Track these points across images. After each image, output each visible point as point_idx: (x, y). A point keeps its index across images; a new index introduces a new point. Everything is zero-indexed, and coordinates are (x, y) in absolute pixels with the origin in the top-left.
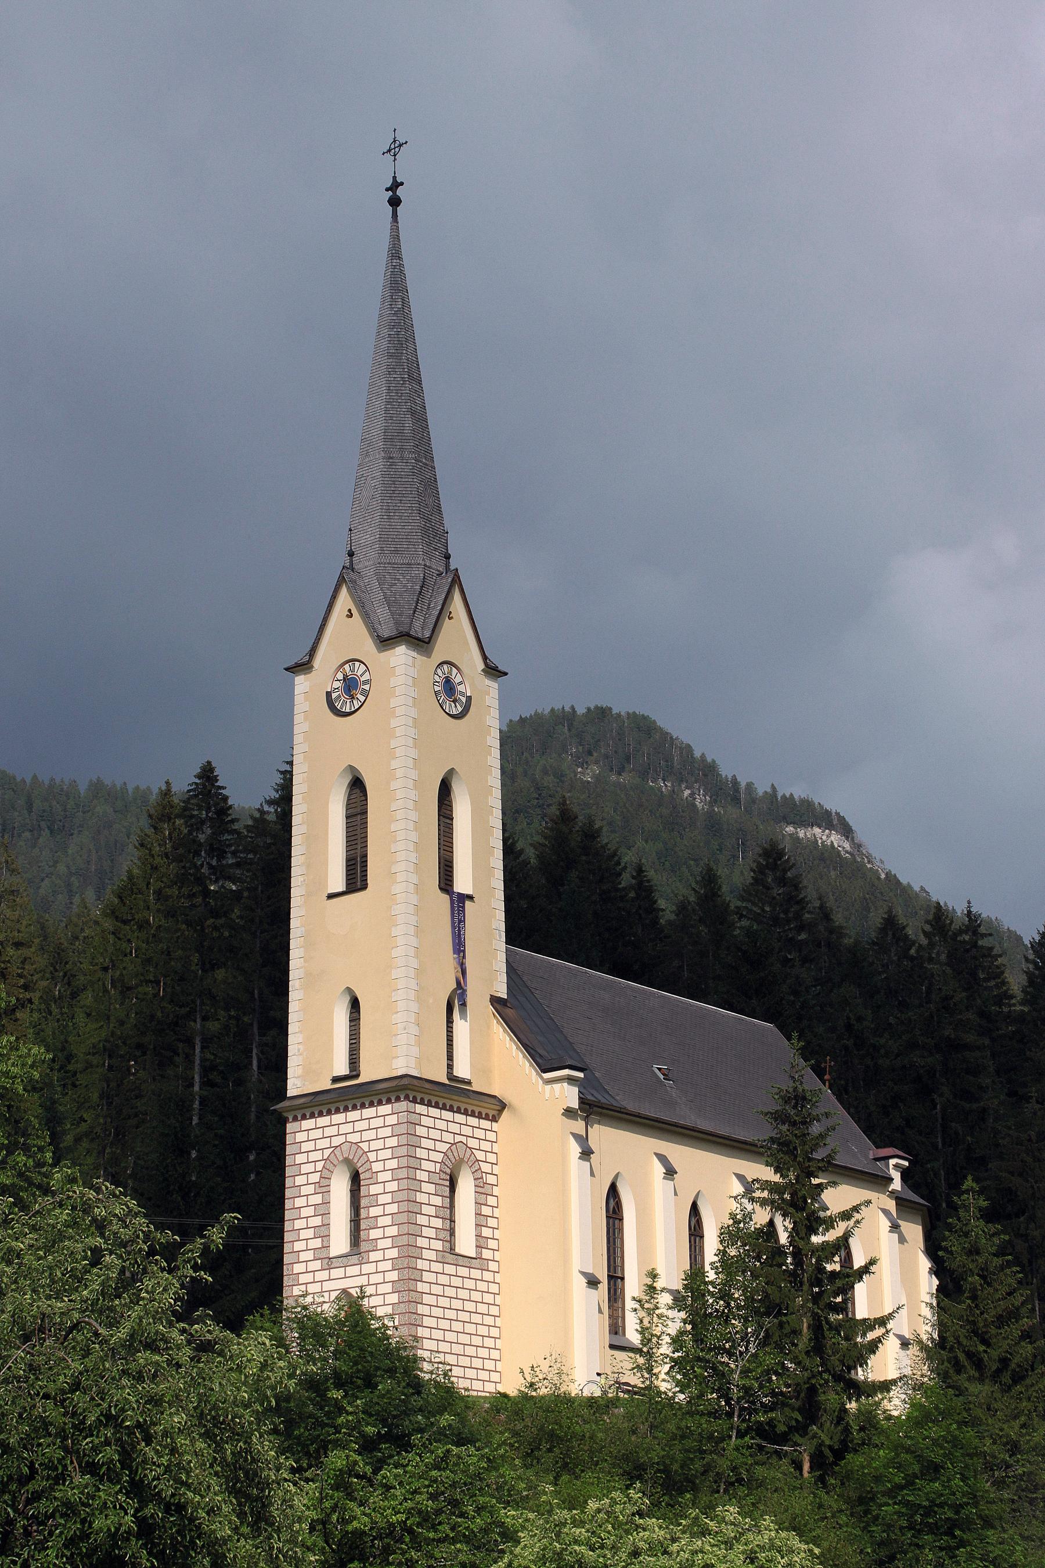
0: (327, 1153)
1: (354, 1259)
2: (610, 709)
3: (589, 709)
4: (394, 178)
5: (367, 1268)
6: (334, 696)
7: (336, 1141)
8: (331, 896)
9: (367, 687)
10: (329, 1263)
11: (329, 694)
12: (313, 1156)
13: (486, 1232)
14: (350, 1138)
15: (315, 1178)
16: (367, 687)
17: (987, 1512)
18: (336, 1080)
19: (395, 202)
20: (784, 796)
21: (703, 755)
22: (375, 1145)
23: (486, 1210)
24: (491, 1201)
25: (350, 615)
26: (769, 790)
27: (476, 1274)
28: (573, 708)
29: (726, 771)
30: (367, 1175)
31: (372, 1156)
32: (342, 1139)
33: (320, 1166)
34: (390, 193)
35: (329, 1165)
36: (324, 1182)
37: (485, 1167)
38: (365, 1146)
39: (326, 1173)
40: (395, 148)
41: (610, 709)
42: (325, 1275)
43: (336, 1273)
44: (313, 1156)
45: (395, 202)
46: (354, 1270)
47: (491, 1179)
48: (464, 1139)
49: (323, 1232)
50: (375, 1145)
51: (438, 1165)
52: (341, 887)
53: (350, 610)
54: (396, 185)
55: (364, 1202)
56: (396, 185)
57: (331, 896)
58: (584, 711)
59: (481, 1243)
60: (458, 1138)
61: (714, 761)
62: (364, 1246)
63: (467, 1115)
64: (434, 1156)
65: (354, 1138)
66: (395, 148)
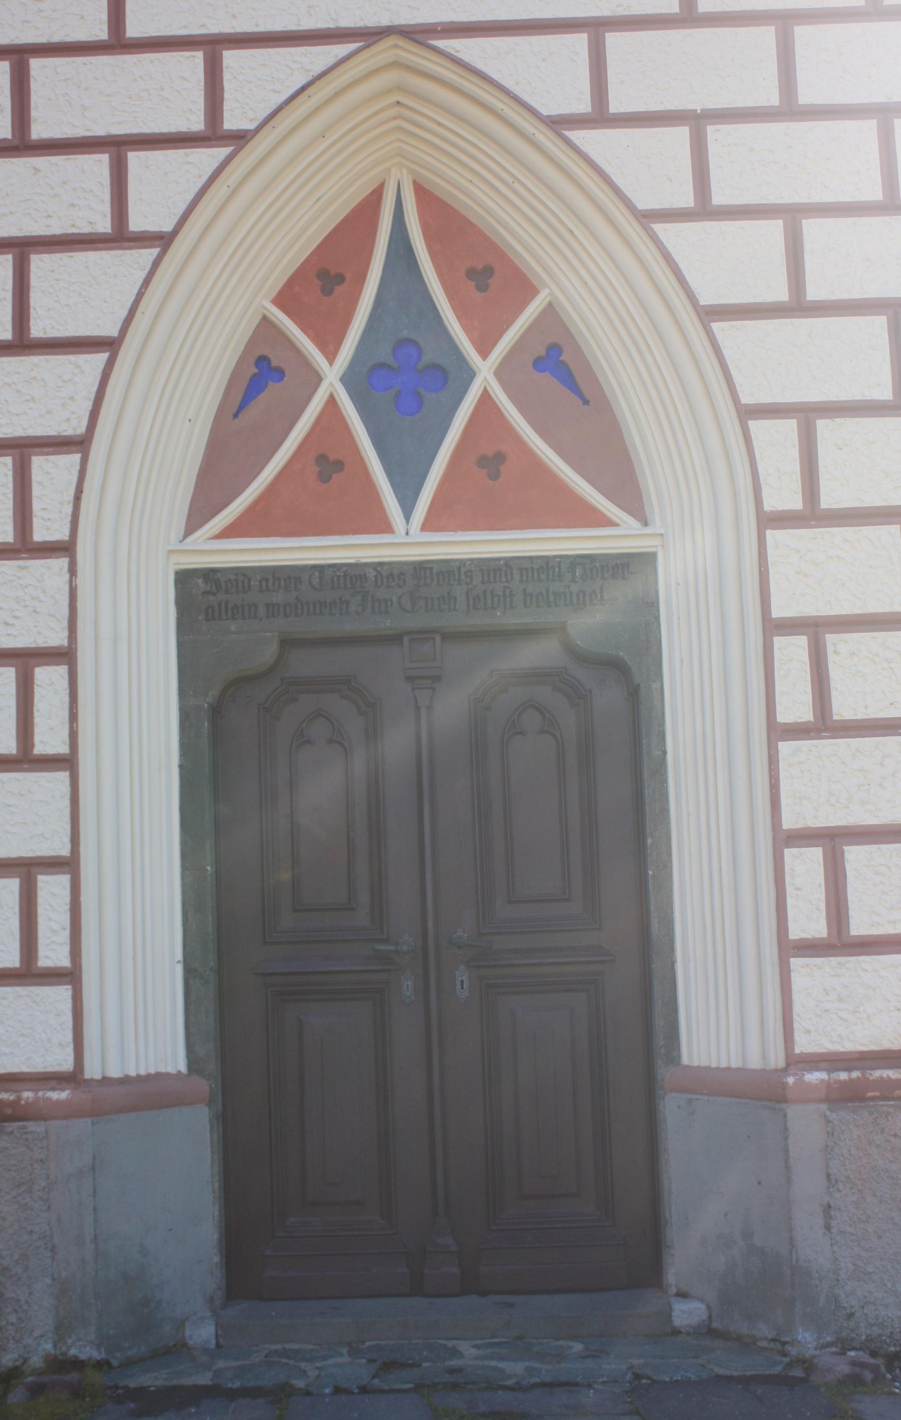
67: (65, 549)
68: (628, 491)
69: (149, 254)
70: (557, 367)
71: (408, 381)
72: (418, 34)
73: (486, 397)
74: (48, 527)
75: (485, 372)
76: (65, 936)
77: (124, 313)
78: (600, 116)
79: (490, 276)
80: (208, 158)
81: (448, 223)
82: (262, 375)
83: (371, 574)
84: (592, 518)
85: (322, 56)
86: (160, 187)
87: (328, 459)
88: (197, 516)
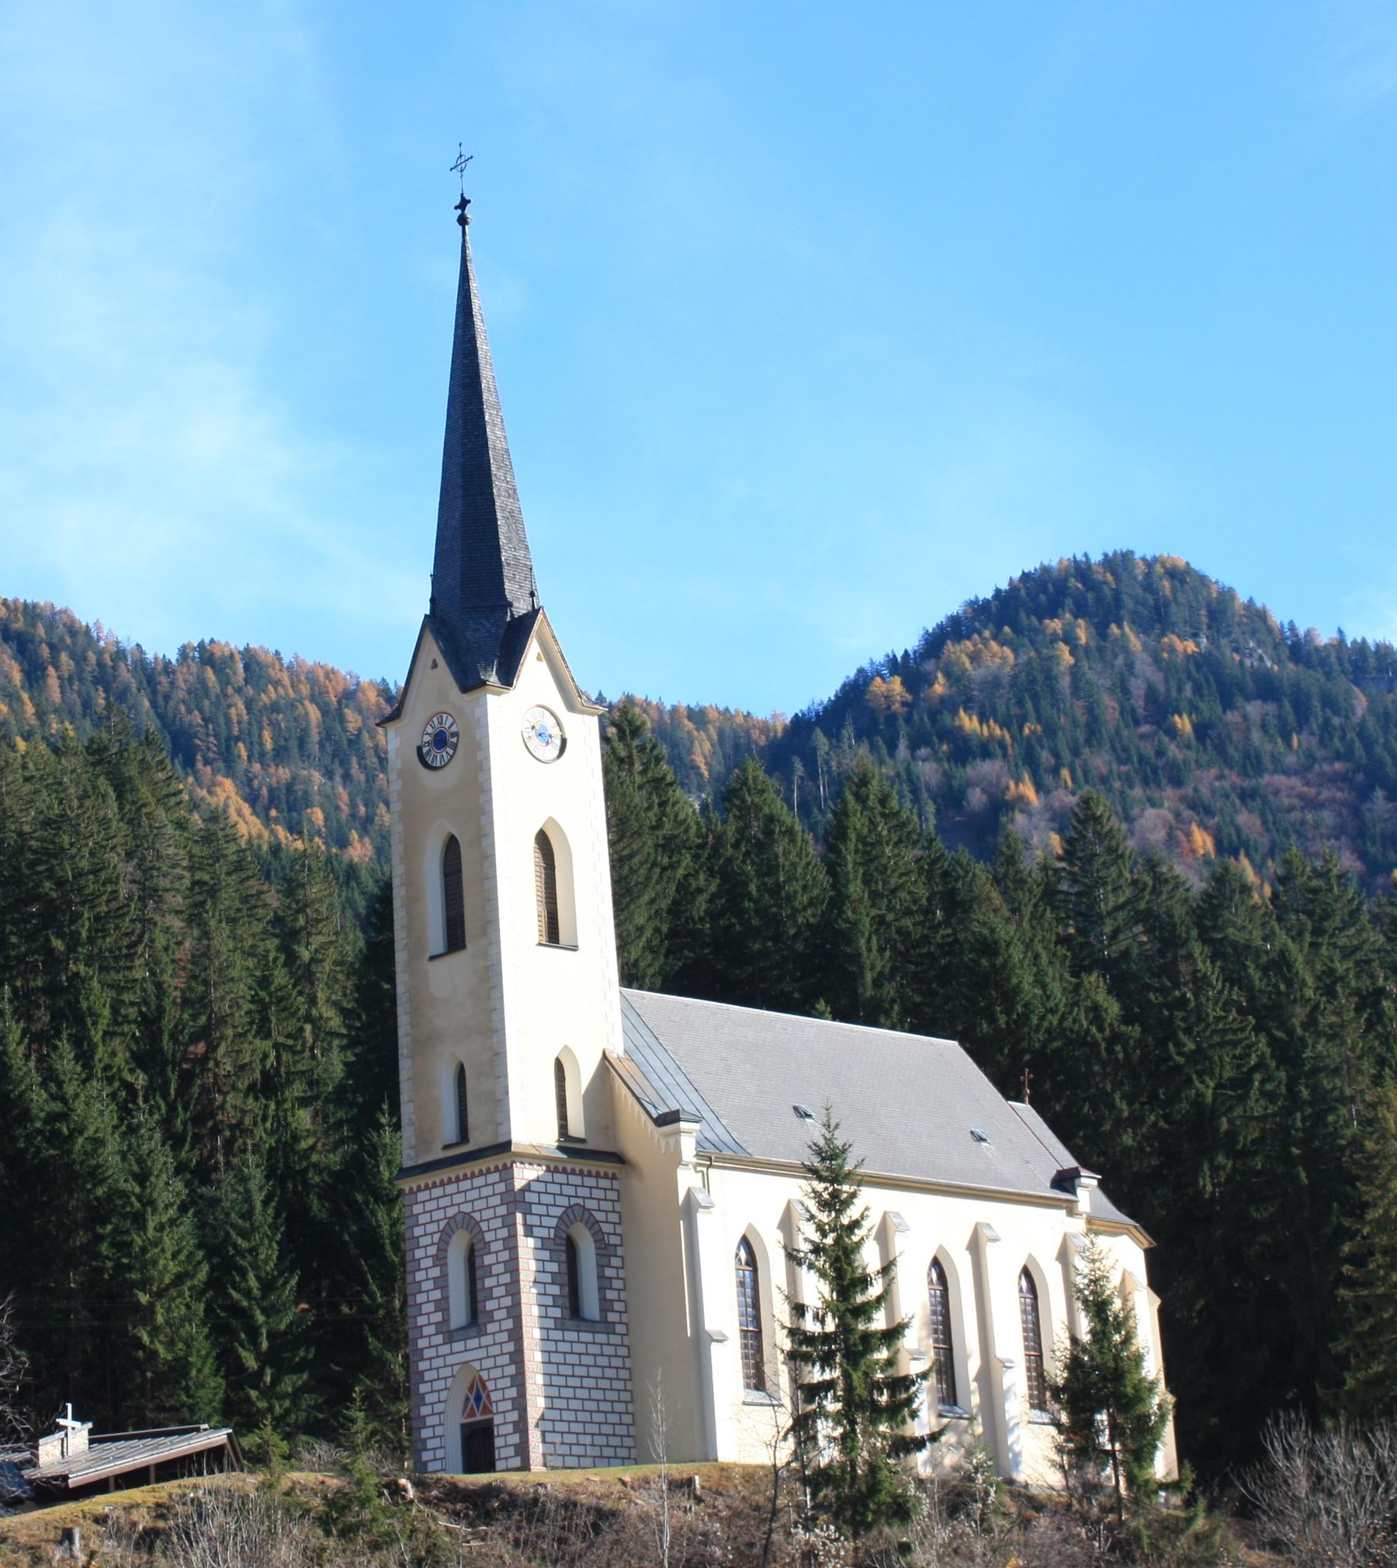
0: (442, 1224)
1: (473, 1331)
2: (1132, 553)
3: (1106, 555)
5: (486, 1340)
6: (425, 750)
7: (451, 1212)
8: (432, 958)
9: (454, 740)
11: (419, 749)
13: (610, 1295)
15: (433, 1250)
16: (454, 740)
18: (446, 1147)
19: (463, 221)
20: (1354, 642)
21: (1251, 600)
22: (487, 1214)
23: (609, 1272)
24: (615, 1262)
25: (435, 665)
26: (1335, 635)
27: (601, 1338)
28: (1086, 555)
29: (1279, 617)
30: (481, 1245)
33: (436, 1237)
34: (459, 212)
35: (445, 1237)
36: (442, 1254)
37: (607, 1228)
38: (476, 1216)
39: (443, 1245)
40: (461, 164)
41: (1132, 553)
43: (458, 1346)
45: (463, 221)
46: (472, 1343)
47: (614, 1240)
48: (580, 1201)
49: (442, 1305)
50: (487, 1214)
51: (552, 1232)
53: (434, 661)
54: (464, 203)
55: (479, 1273)
56: (464, 203)
57: (432, 958)
58: (1100, 558)
59: (606, 1305)
60: (573, 1201)
62: (481, 1319)
64: (546, 1221)
65: (466, 1208)
66: (461, 164)
71: (478, 1398)
82: (467, 1399)
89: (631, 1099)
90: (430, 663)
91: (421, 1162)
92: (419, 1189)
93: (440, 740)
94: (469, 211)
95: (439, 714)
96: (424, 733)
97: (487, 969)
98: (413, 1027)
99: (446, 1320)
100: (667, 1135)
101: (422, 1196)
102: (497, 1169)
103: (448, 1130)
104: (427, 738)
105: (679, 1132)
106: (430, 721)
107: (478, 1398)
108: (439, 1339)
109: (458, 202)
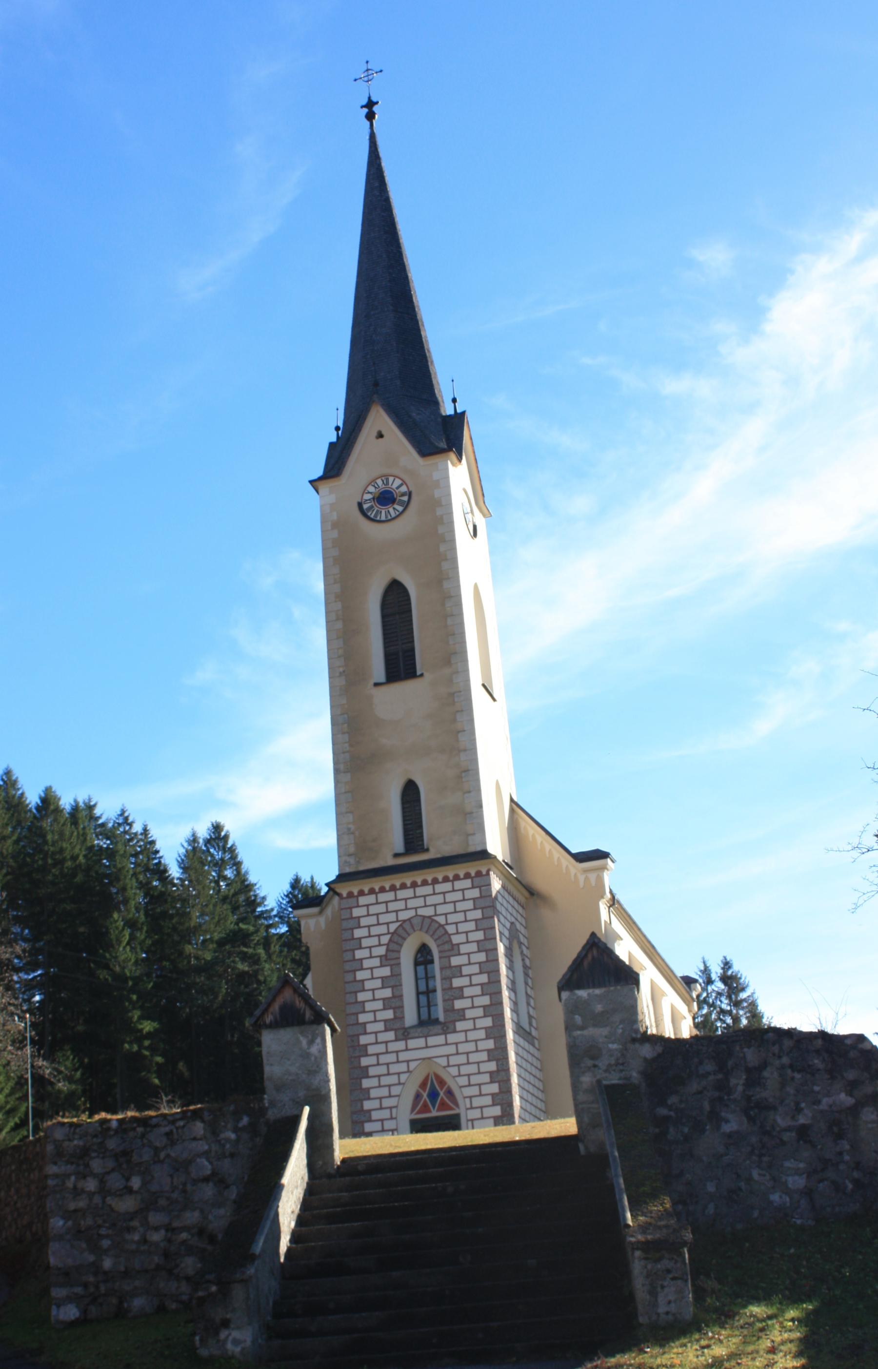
0: (393, 927)
4: (369, 98)
5: (452, 1038)
6: (365, 506)
7: (404, 915)
8: (376, 685)
10: (404, 1034)
11: (360, 505)
12: (375, 931)
14: (421, 912)
17: (290, 1078)
18: (396, 855)
31: (451, 929)
32: (412, 913)
33: (385, 939)
35: (396, 938)
38: (441, 920)
39: (393, 946)
40: (368, 75)
42: (401, 1045)
43: (412, 1043)
44: (375, 931)
45: (370, 116)
49: (394, 1003)
52: (382, 679)
54: (370, 104)
57: (376, 685)
61: (17, 778)
63: (376, 894)
66: (368, 75)
67: (396, 1118)
68: (457, 1105)
69: (397, 1098)
70: (450, 1093)
71: (433, 1095)
72: (429, 1058)
73: (442, 1099)
74: (394, 1116)
75: (442, 1094)
76: (417, 1051)
77: (543, 833)
78: (449, 1066)
79: (442, 1082)
80: (407, 1074)
81: (437, 1077)
82: (418, 1096)
83: (344, 858)
84: (452, 1109)
85: (419, 1062)
86: (403, 1078)
87: (425, 1105)
88: (413, 1110)
89: (540, 836)
90: (375, 434)
91: (361, 868)
92: (361, 893)
93: (386, 498)
94: (375, 109)
95: (385, 477)
96: (365, 491)
97: (452, 695)
98: (351, 746)
99: (399, 1017)
100: (586, 871)
101: (363, 900)
102: (467, 876)
103: (396, 839)
104: (367, 497)
105: (604, 868)
106: (373, 482)
107: (433, 1095)
108: (391, 1035)
109: (365, 101)
